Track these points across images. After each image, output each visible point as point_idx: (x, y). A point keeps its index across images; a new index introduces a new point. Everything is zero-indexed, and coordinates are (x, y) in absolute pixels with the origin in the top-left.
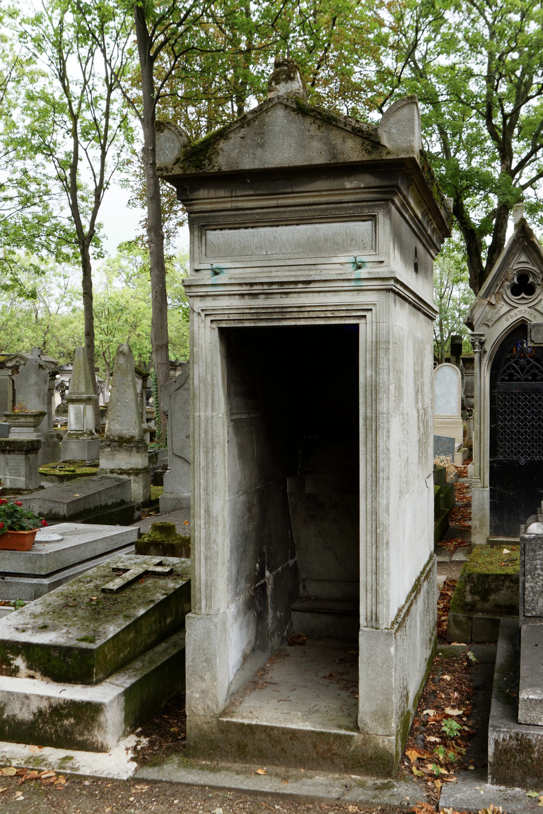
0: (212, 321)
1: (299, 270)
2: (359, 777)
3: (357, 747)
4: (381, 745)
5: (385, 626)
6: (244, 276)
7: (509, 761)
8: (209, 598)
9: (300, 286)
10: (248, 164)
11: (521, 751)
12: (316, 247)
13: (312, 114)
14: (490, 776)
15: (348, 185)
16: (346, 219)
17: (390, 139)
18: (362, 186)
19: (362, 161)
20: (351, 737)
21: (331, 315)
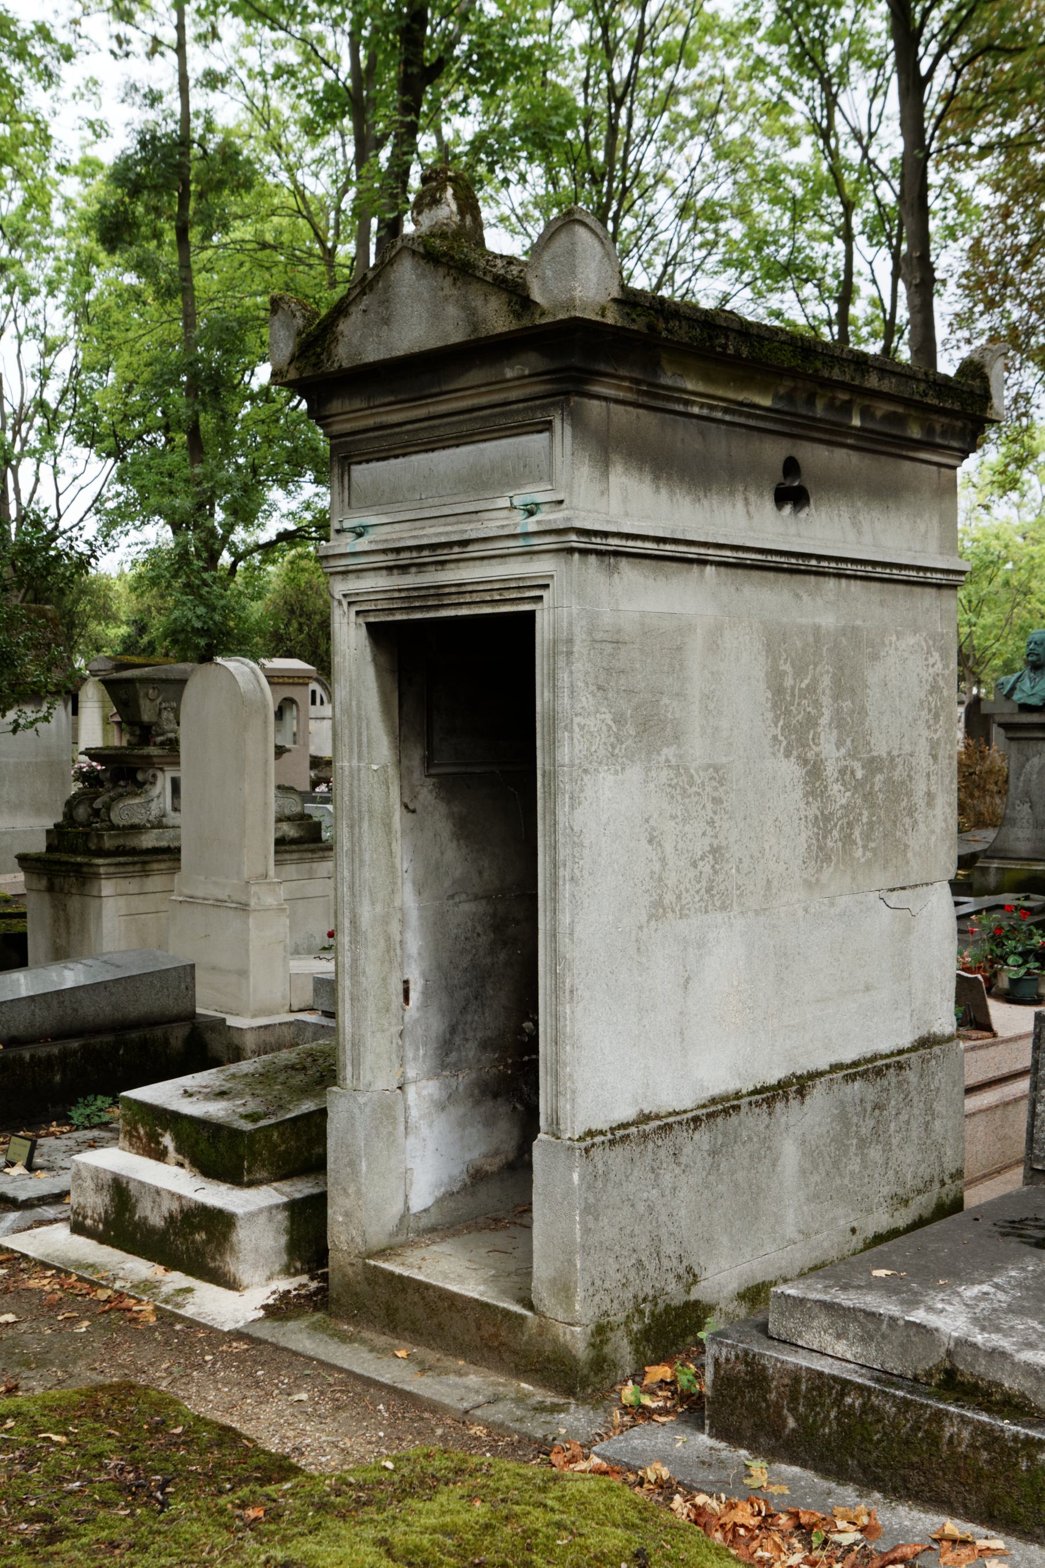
0: (358, 613)
1: (457, 523)
2: (531, 1388)
3: (530, 1337)
4: (561, 1339)
5: (568, 1135)
6: (389, 537)
7: (734, 1399)
8: (357, 1064)
9: (456, 550)
10: (372, 354)
11: (751, 1385)
12: (481, 482)
13: (444, 260)
14: (707, 1422)
15: (509, 374)
16: (515, 431)
17: (544, 289)
18: (527, 372)
19: (510, 332)
20: (523, 1318)
21: (498, 598)
